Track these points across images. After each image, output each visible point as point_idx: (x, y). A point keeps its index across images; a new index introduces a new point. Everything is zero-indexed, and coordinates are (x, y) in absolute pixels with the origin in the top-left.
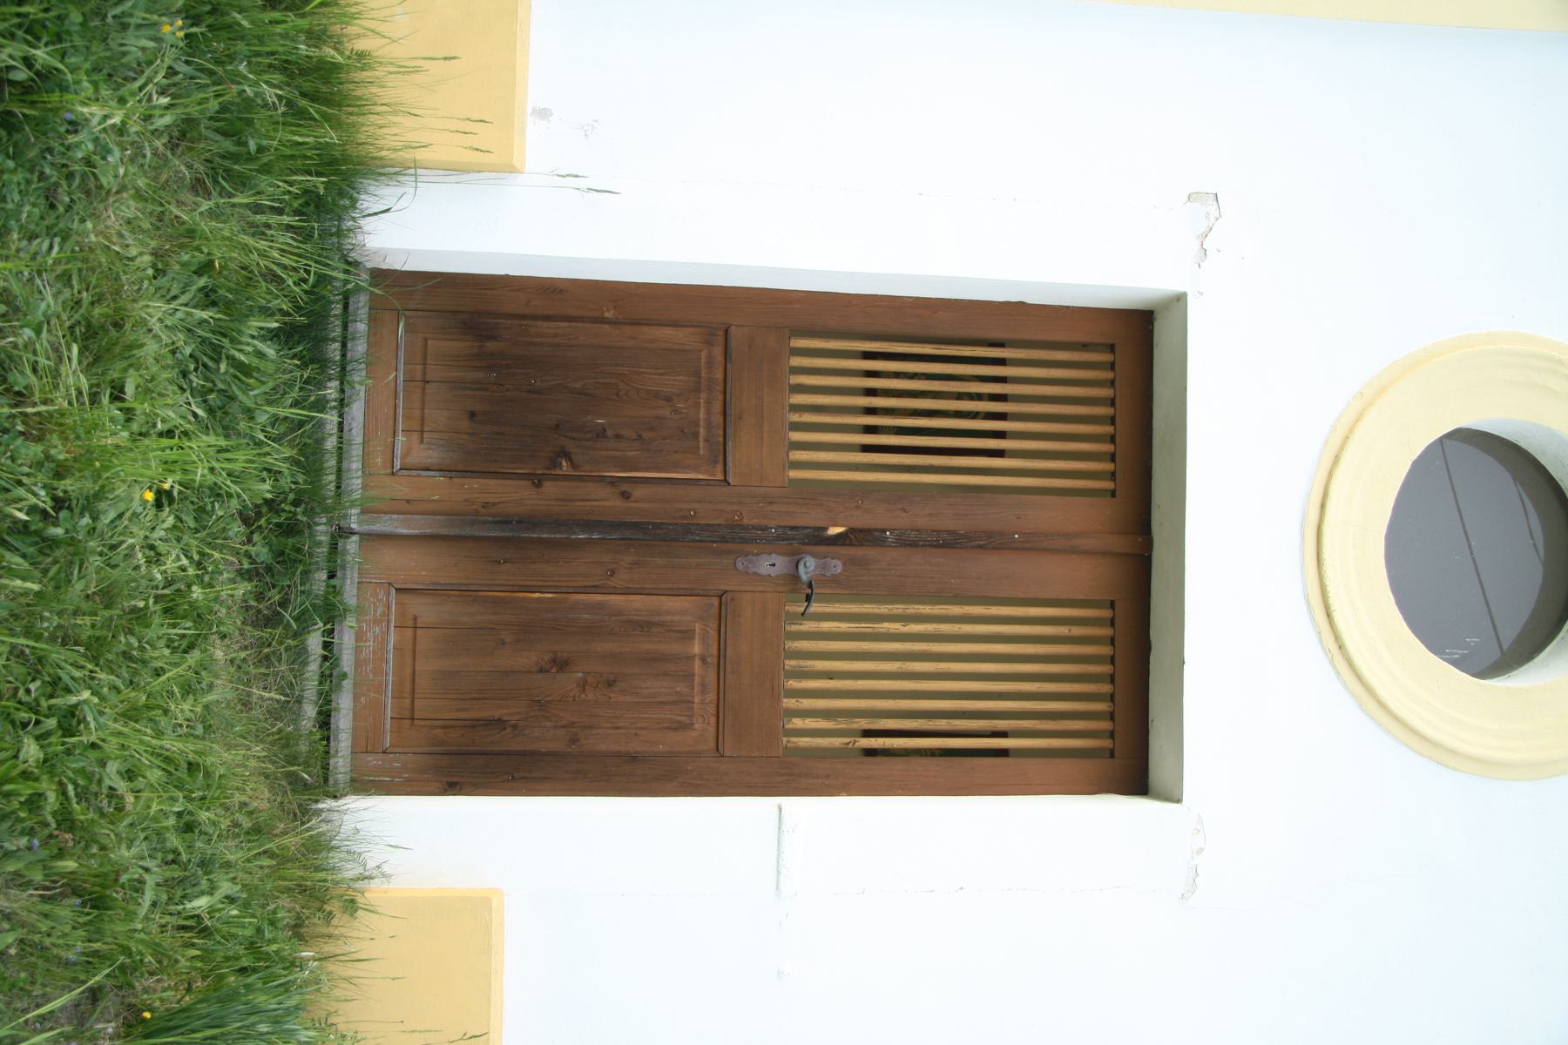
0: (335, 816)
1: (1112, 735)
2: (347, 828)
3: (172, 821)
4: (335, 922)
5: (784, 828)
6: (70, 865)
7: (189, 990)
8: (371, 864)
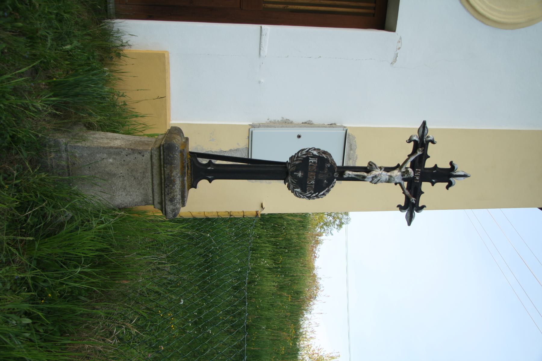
0: (111, 25)
1: (374, 9)
2: (115, 29)
3: (54, 16)
4: (114, 60)
5: (263, 34)
6: (20, 24)
7: (67, 73)
8: (124, 41)
